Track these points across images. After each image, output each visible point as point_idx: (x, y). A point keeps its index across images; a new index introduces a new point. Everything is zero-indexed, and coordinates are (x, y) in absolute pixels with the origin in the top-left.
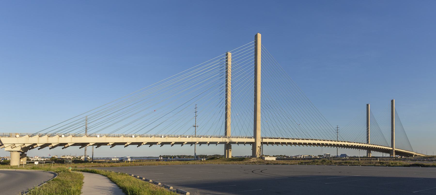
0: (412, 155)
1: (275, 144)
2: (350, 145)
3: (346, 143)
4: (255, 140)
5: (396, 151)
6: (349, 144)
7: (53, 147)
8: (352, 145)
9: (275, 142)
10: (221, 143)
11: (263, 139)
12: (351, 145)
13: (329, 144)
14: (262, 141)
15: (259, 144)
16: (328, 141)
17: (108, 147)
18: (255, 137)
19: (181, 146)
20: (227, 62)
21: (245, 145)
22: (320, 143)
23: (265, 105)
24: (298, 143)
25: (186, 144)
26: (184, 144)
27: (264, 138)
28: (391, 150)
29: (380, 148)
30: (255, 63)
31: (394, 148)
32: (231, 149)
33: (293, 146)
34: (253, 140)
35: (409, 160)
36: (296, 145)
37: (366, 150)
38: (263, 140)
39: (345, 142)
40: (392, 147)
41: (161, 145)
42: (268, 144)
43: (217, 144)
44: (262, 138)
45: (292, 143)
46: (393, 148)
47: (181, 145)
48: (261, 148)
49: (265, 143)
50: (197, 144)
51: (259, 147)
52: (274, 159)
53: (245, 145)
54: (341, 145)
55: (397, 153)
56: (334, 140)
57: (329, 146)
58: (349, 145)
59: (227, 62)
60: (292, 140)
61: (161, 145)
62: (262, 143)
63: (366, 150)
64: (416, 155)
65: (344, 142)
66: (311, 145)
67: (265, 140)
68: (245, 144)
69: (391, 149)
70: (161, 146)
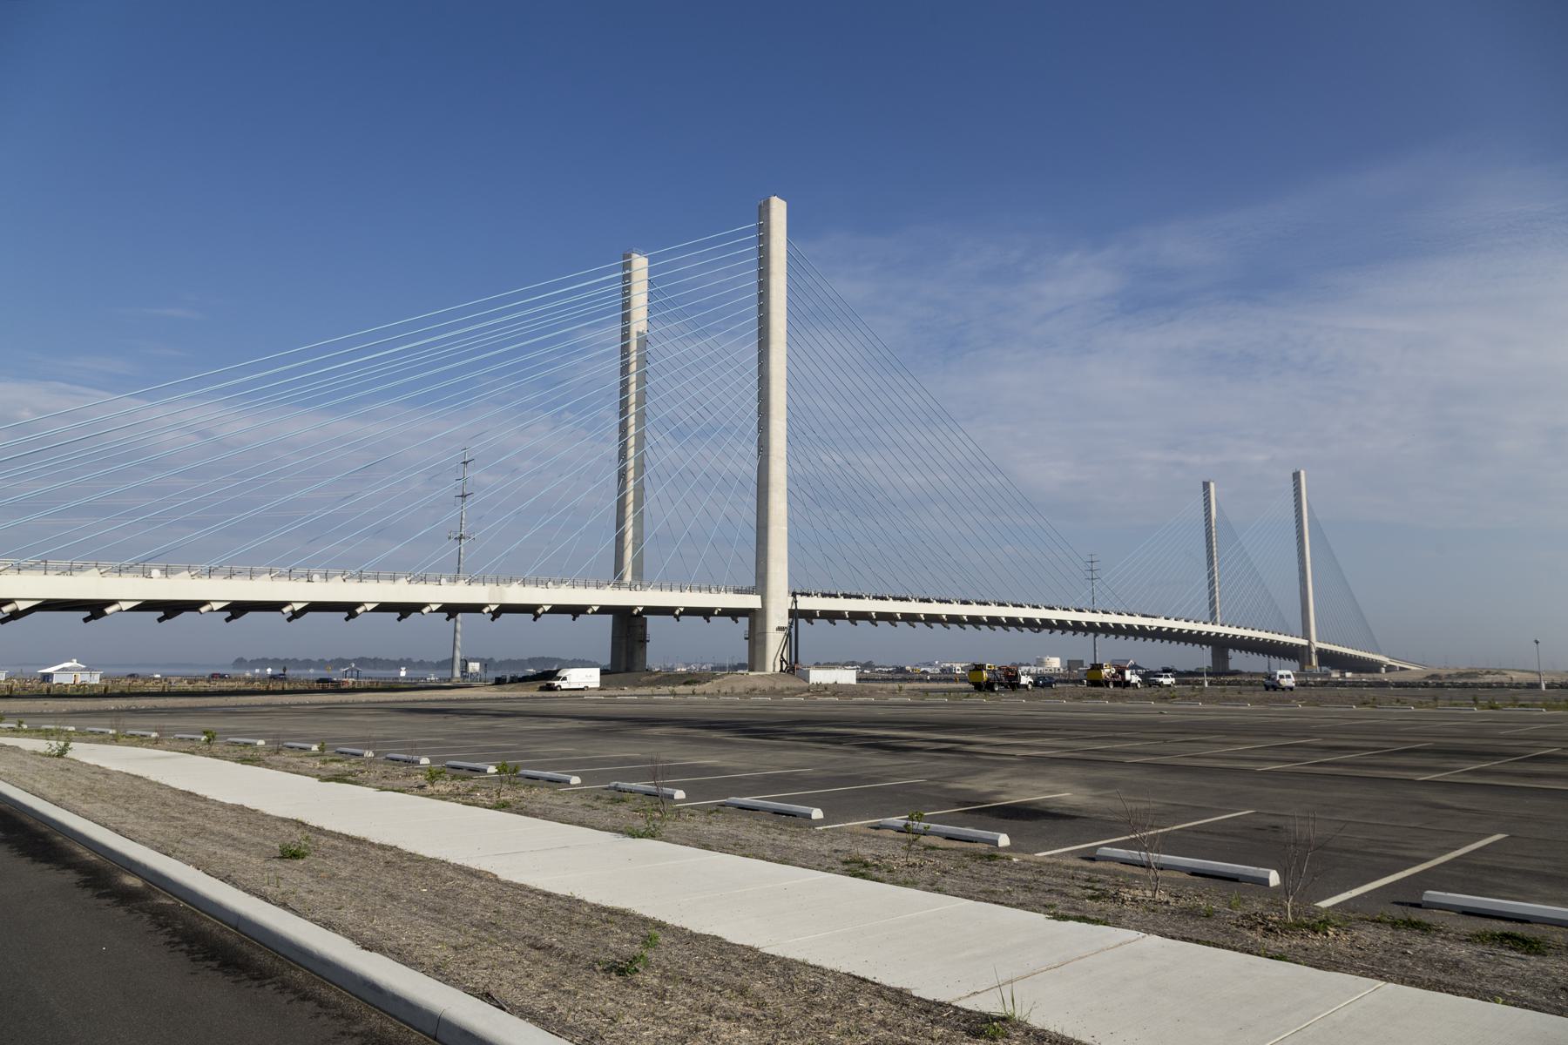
0: (1374, 667)
1: (821, 617)
2: (1150, 627)
3: (1137, 621)
4: (764, 602)
5: (1320, 652)
6: (1147, 622)
7: (296, 615)
8: (1159, 628)
9: (822, 612)
10: (604, 610)
11: (798, 597)
12: (1155, 628)
13: (1041, 620)
14: (794, 607)
15: (777, 617)
16: (1065, 609)
17: (485, 617)
18: (760, 585)
19: (399, 619)
20: (627, 272)
21: (681, 618)
22: (1034, 619)
23: (801, 458)
24: (925, 615)
25: (550, 611)
26: (359, 610)
27: (802, 594)
28: (1303, 646)
29: (1257, 638)
30: (760, 318)
31: (1314, 638)
32: (789, 610)
33: (969, 627)
34: (753, 602)
35: (1362, 686)
36: (915, 624)
37: (1210, 647)
38: (796, 602)
39: (1132, 615)
40: (1306, 635)
41: (228, 614)
42: (877, 619)
43: (537, 616)
44: (794, 595)
45: (898, 615)
46: (1310, 642)
47: (346, 614)
48: (792, 637)
49: (809, 615)
50: (593, 613)
51: (780, 629)
52: (848, 677)
53: (681, 618)
54: (1117, 626)
55: (1327, 658)
56: (1060, 604)
57: (1057, 627)
58: (1148, 628)
59: (627, 272)
60: (922, 604)
61: (228, 614)
62: (795, 614)
63: (1210, 647)
64: (1390, 665)
65: (1129, 615)
66: (983, 623)
67: (805, 603)
68: (677, 617)
69: (1304, 642)
70: (228, 620)
